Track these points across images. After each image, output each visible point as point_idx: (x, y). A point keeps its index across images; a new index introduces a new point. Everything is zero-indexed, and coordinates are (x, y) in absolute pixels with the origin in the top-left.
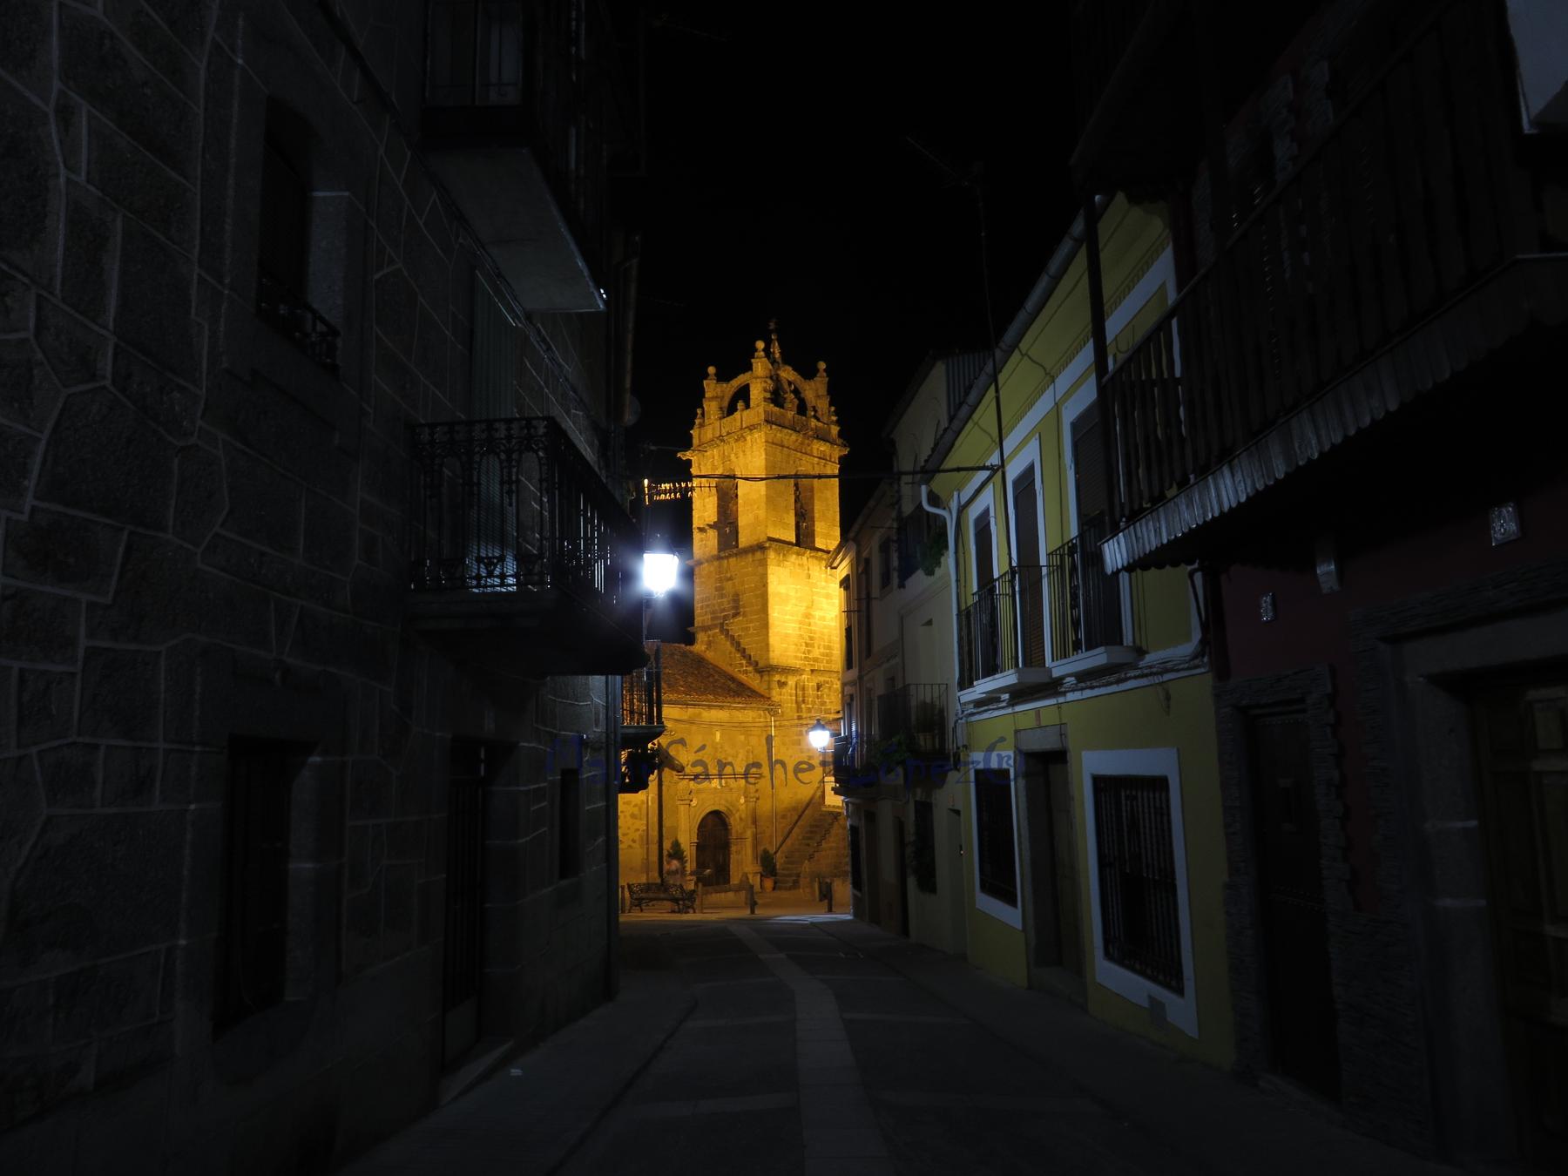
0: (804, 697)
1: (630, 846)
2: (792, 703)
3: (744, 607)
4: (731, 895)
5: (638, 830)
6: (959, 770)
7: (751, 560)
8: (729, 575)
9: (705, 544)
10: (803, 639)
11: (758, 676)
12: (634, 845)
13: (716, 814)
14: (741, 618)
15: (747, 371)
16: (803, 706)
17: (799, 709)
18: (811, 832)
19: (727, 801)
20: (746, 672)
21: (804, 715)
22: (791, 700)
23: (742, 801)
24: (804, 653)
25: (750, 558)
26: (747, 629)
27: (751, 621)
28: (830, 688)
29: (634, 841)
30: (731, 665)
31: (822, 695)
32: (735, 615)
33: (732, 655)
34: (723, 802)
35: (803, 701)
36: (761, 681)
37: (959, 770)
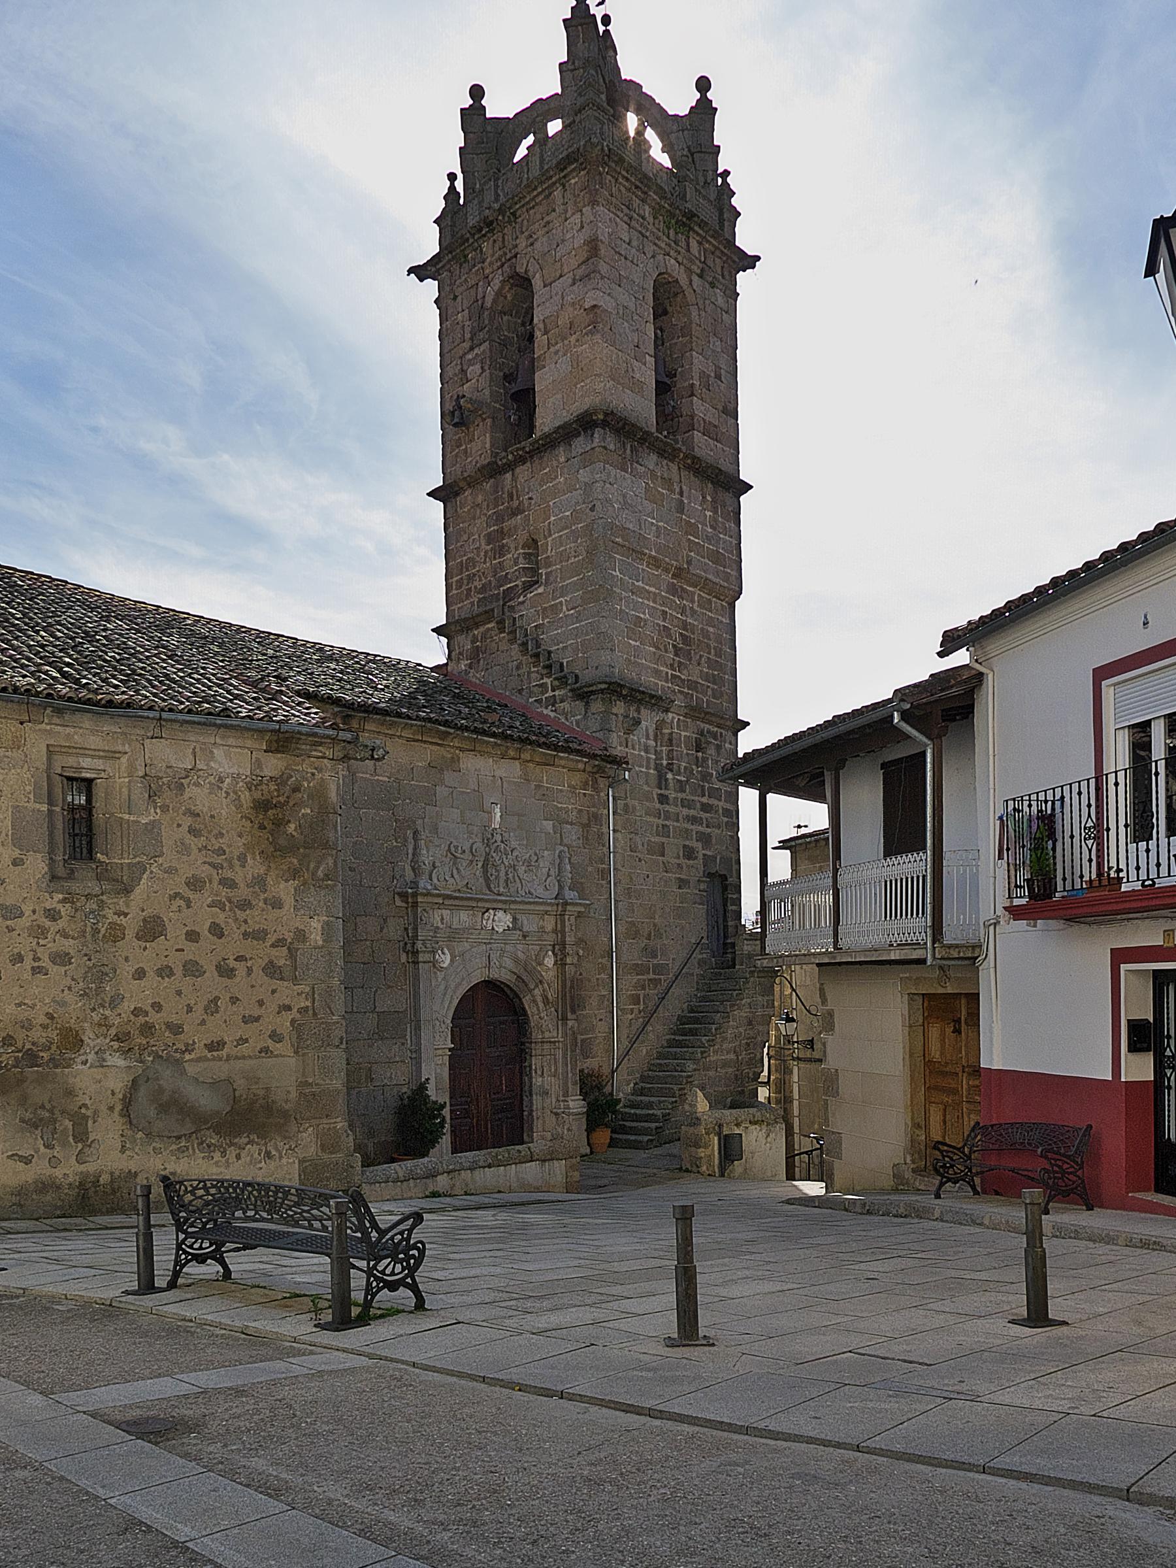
0: (670, 758)
1: (265, 1050)
2: (648, 768)
3: (548, 565)
4: (531, 1170)
5: (288, 1008)
6: (953, 1032)
7: (562, 459)
8: (515, 503)
9: (465, 451)
10: (669, 636)
11: (580, 704)
12: (277, 1048)
13: (490, 986)
14: (540, 590)
15: (917, 851)
16: (670, 776)
17: (661, 781)
18: (693, 1032)
19: (516, 960)
20: (553, 702)
21: (672, 794)
22: (648, 759)
23: (549, 961)
24: (672, 667)
25: (561, 454)
26: (555, 609)
27: (564, 591)
28: (718, 747)
29: (275, 1037)
30: (520, 691)
31: (705, 760)
32: (528, 586)
33: (524, 670)
34: (508, 963)
35: (670, 767)
36: (585, 717)
37: (953, 1032)
